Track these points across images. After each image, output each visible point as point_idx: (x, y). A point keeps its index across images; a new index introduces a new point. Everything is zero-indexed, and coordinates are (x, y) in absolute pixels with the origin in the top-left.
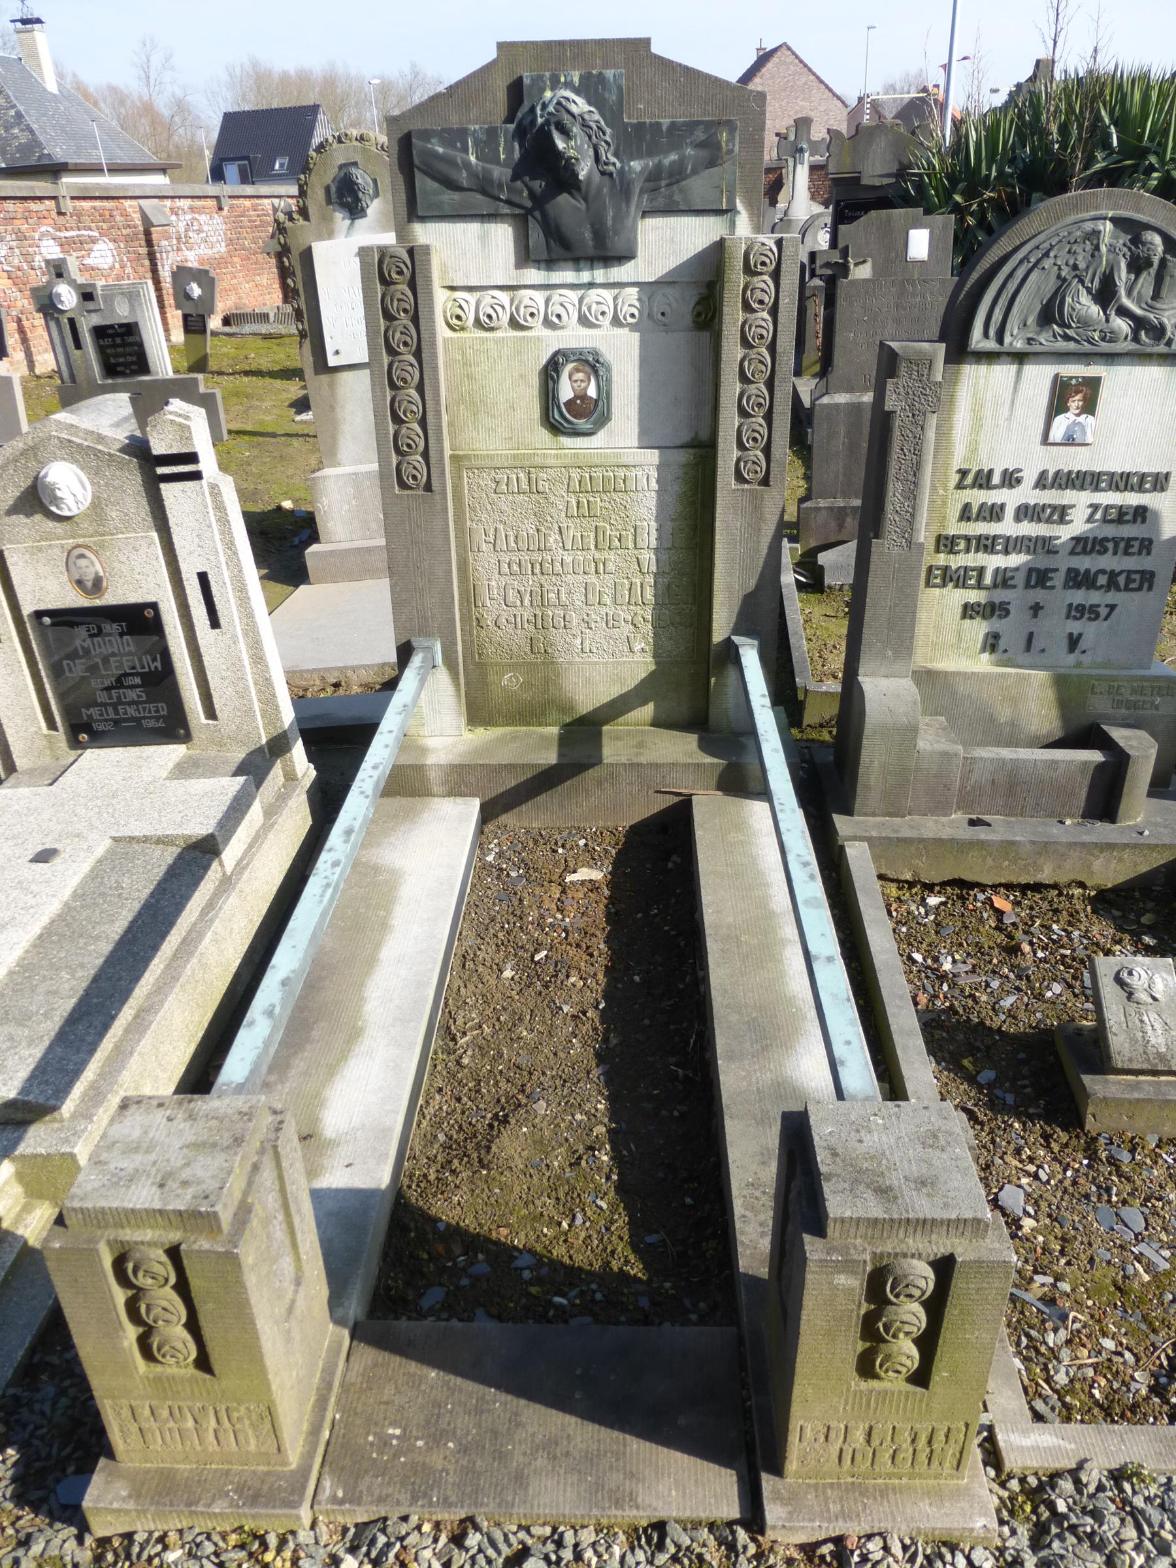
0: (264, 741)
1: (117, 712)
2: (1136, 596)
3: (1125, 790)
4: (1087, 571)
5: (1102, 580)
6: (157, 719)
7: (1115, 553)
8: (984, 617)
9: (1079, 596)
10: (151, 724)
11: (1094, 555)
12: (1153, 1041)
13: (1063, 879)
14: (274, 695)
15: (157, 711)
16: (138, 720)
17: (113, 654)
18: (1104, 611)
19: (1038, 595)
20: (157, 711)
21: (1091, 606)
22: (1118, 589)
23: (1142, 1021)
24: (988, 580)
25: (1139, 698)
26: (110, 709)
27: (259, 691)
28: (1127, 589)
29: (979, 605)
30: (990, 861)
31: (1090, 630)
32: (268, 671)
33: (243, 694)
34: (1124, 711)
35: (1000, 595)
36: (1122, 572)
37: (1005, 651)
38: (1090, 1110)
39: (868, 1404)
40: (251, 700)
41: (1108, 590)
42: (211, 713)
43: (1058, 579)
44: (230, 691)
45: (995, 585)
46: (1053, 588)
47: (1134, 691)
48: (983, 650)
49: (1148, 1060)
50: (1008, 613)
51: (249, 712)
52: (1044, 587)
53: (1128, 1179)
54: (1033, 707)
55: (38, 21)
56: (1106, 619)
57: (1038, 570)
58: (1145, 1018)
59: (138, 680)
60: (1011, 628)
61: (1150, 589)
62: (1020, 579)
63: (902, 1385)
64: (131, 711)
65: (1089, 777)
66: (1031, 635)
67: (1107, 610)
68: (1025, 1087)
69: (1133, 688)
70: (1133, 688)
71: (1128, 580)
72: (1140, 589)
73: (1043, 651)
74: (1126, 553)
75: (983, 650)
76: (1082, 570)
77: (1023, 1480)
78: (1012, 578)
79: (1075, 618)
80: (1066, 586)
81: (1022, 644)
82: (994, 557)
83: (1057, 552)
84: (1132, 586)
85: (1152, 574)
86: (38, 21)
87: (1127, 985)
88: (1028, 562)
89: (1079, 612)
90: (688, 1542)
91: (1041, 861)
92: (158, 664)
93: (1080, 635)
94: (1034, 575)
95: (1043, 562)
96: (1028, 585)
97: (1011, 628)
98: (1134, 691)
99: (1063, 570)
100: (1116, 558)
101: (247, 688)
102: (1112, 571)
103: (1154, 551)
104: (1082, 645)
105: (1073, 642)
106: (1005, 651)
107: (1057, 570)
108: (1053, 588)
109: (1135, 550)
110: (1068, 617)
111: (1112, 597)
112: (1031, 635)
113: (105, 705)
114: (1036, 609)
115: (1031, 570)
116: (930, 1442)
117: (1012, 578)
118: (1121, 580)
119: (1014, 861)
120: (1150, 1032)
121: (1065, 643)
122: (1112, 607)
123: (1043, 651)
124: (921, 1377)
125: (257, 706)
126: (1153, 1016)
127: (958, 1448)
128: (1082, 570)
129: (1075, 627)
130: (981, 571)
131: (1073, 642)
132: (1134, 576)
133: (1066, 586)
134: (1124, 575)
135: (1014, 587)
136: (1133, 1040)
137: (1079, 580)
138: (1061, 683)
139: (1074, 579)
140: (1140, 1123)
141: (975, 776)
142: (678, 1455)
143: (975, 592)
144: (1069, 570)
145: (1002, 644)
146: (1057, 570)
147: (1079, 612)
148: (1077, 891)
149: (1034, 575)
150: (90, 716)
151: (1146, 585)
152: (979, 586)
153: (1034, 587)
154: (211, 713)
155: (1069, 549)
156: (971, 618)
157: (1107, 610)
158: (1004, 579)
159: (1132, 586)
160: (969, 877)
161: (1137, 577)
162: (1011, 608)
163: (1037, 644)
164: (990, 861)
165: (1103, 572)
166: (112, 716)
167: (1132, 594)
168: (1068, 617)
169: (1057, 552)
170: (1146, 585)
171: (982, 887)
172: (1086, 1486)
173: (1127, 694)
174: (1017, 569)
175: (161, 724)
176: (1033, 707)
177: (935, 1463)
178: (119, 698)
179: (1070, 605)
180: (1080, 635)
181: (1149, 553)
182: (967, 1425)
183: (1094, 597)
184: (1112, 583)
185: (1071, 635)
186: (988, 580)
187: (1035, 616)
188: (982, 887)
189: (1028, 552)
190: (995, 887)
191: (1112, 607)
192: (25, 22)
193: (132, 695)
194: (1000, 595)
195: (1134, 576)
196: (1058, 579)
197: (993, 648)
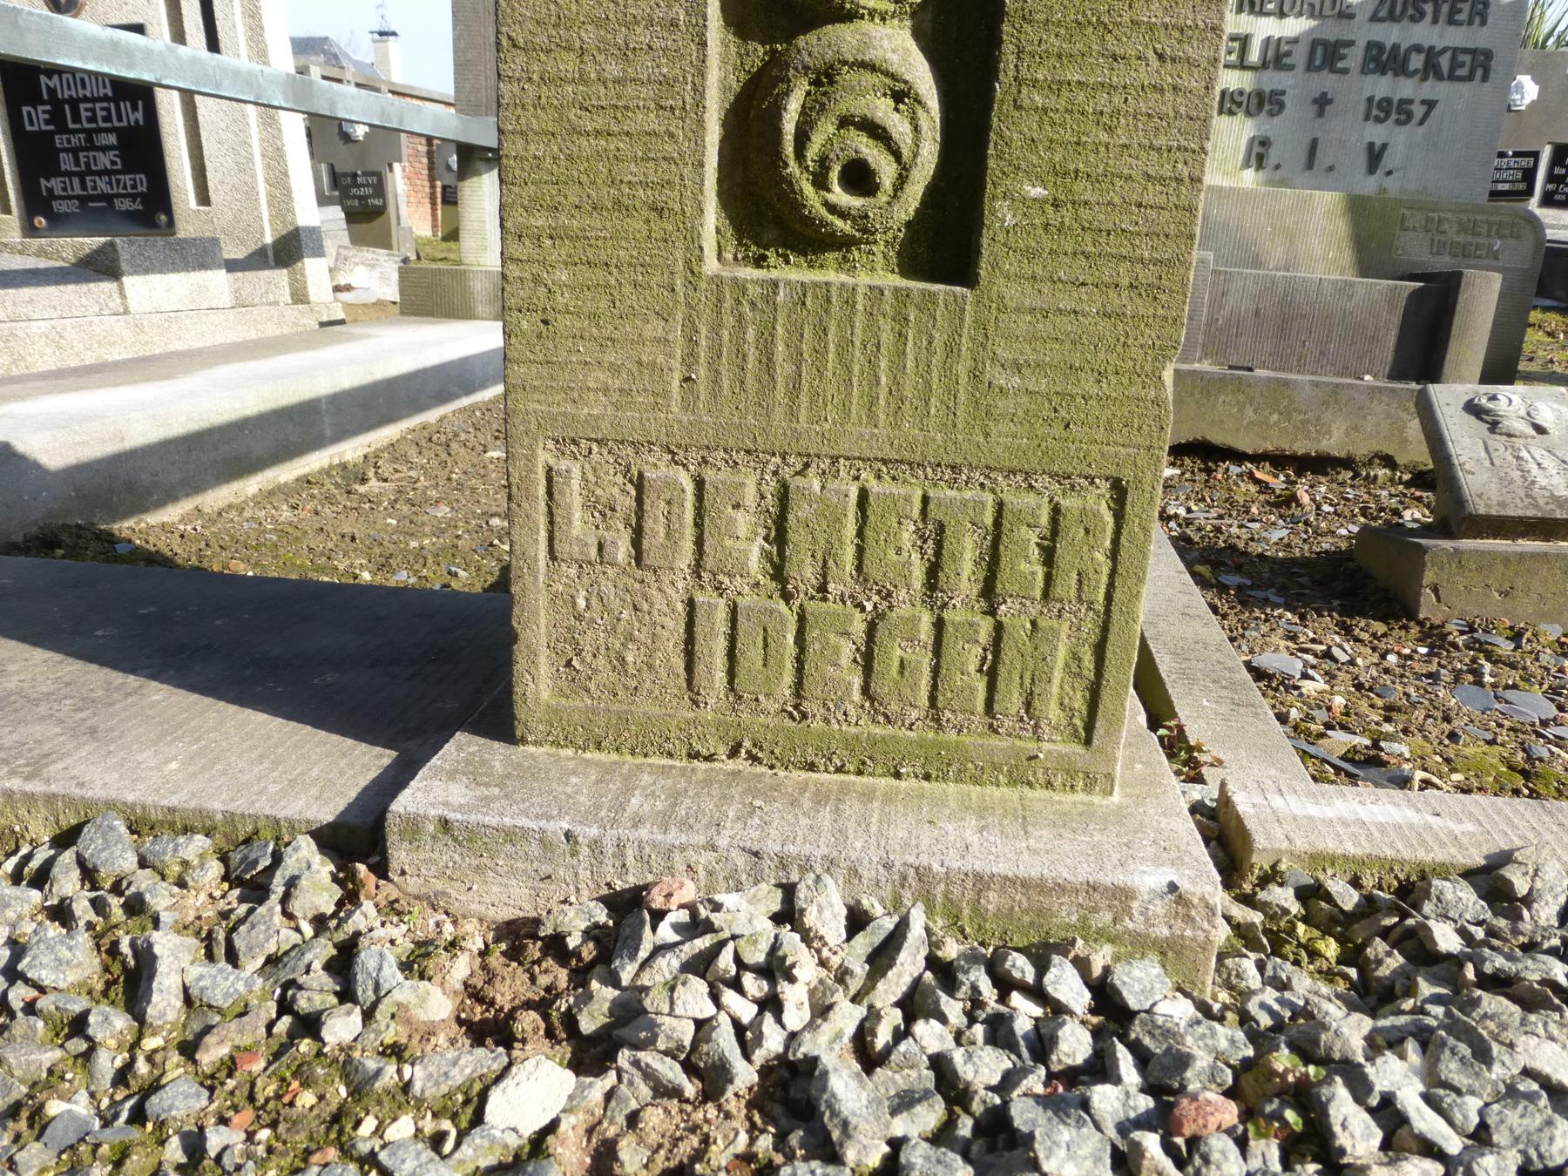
0: (269, 239)
1: (84, 186)
2: (1465, 88)
3: (1455, 330)
4: (1396, 47)
5: (1417, 62)
6: (133, 197)
7: (1435, 21)
8: (1248, 113)
9: (1382, 86)
10: (124, 205)
11: (1405, 22)
12: (1542, 481)
13: (1361, 450)
14: (286, 174)
15: (134, 187)
16: (108, 198)
17: (85, 99)
18: (1418, 111)
19: (1326, 81)
20: (134, 187)
21: (1402, 102)
22: (1439, 77)
23: (1518, 458)
24: (1254, 56)
25: (1469, 239)
26: (76, 180)
27: (268, 167)
28: (1452, 77)
29: (1241, 93)
30: (1249, 412)
31: (1398, 139)
32: (280, 138)
33: (245, 167)
34: (1447, 259)
35: (1273, 80)
36: (1445, 50)
37: (1277, 167)
38: (1429, 577)
39: (768, 364)
40: (254, 176)
41: (1424, 79)
42: (204, 198)
43: (1353, 59)
44: (229, 163)
45: (1264, 65)
46: (1345, 71)
47: (1462, 228)
48: (1246, 164)
49: (1536, 506)
50: (1282, 106)
51: (250, 194)
52: (1334, 70)
53: (1512, 666)
54: (1317, 246)
55: (394, 34)
56: (1421, 123)
57: (1324, 44)
58: (1524, 454)
59: (112, 139)
60: (1288, 129)
61: (1485, 78)
62: (1299, 56)
63: (876, 274)
64: (102, 185)
65: (1400, 312)
66: (1314, 144)
67: (1423, 109)
68: (1300, 575)
69: (1460, 223)
70: (1460, 223)
71: (1455, 64)
72: (1470, 78)
73: (1331, 168)
74: (1451, 21)
75: (1246, 164)
76: (1388, 46)
77: (1311, 894)
78: (1288, 54)
79: (1378, 120)
80: (1364, 71)
81: (1302, 157)
82: (1263, 21)
83: (1351, 17)
84: (1459, 72)
85: (1488, 55)
86: (394, 34)
87: (1487, 412)
88: (1311, 30)
89: (1383, 110)
90: (129, 862)
91: (1327, 416)
92: (140, 116)
93: (1384, 146)
94: (1320, 50)
95: (1333, 32)
96: (1310, 67)
97: (1288, 129)
98: (1462, 228)
99: (1361, 44)
100: (1437, 28)
101: (250, 159)
102: (1431, 48)
103: (1490, 20)
104: (1387, 162)
105: (1375, 156)
106: (1277, 167)
107: (1350, 44)
108: (1345, 71)
109: (1463, 17)
110: (1367, 118)
111: (1432, 89)
112: (1314, 144)
113: (70, 174)
114: (1322, 103)
115: (1315, 44)
116: (989, 591)
117: (1288, 54)
118: (1445, 62)
119: (1286, 414)
120: (1535, 470)
121: (1362, 160)
122: (1430, 105)
123: (1331, 168)
124: (946, 242)
125: (262, 188)
126: (1538, 453)
127: (1090, 629)
128: (1388, 46)
129: (1376, 133)
130: (1244, 41)
131: (1375, 156)
132: (1462, 58)
133: (1364, 71)
134: (1448, 55)
135: (1291, 68)
136: (1505, 481)
137: (1384, 60)
138: (1357, 208)
139: (1376, 59)
140: (1523, 610)
141: (1231, 302)
142: (262, 717)
143: (1237, 73)
144: (1371, 45)
145: (1273, 156)
146: (1350, 44)
147: (1383, 110)
148: (1382, 473)
149: (1320, 50)
150: (50, 191)
151: (1479, 72)
152: (1242, 65)
153: (1319, 69)
154: (204, 198)
155: (1369, 14)
156: (1231, 113)
157: (1423, 109)
158: (1277, 56)
159: (1459, 72)
160: (1218, 437)
161: (1467, 58)
162: (1288, 100)
163: (1324, 157)
164: (1249, 412)
165: (1418, 48)
166: (78, 191)
167: (1457, 86)
168: (1367, 118)
169: (1351, 17)
170: (1479, 72)
171: (1238, 457)
172: (1528, 900)
173: (1452, 234)
174: (1295, 41)
175: (138, 206)
176: (1317, 246)
177: (1011, 700)
178: (88, 164)
179: (1370, 100)
180: (1384, 146)
181: (1483, 23)
182: (1119, 493)
183: (1405, 88)
184: (1431, 68)
185: (1371, 145)
186: (1254, 56)
187: (1321, 114)
188: (1238, 457)
189: (1312, 16)
190: (1257, 459)
191: (1430, 105)
192: (381, 34)
193: (104, 161)
194: (1273, 80)
195: (1462, 58)
196: (1353, 59)
197: (1260, 161)
